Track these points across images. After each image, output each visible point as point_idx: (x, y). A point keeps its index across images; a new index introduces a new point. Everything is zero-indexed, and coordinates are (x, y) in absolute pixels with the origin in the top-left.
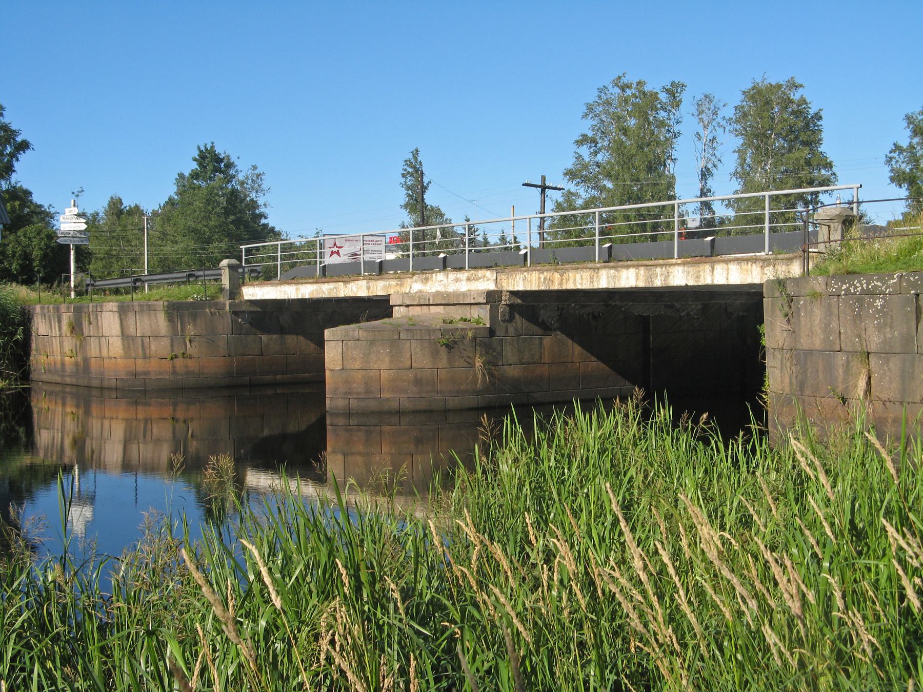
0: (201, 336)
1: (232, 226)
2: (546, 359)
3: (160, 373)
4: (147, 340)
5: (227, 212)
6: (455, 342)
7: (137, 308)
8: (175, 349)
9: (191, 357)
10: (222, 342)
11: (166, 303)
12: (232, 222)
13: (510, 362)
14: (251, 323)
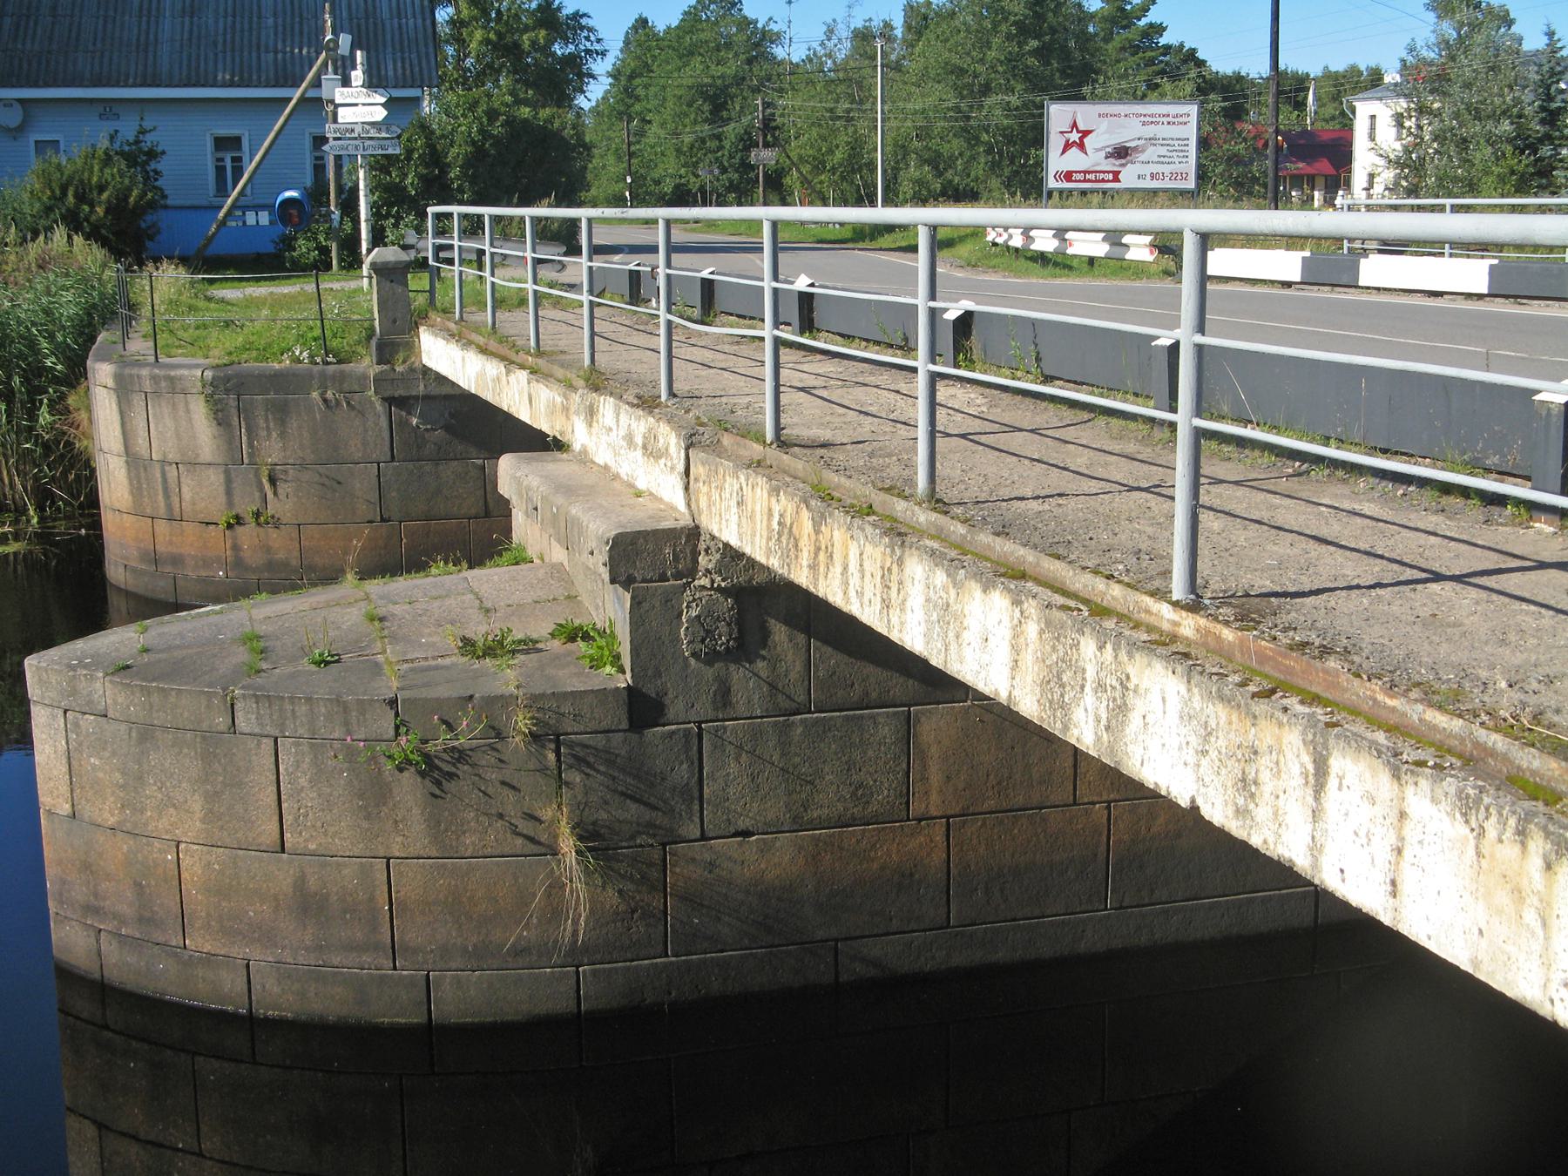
0: (303, 466)
1: (1032, 61)
2: (932, 798)
3: (207, 563)
4: (172, 472)
5: (1024, 31)
6: (460, 755)
7: (148, 386)
8: (237, 499)
9: (276, 523)
10: (362, 484)
11: (209, 374)
12: (1036, 53)
13: (743, 824)
14: (447, 428)
